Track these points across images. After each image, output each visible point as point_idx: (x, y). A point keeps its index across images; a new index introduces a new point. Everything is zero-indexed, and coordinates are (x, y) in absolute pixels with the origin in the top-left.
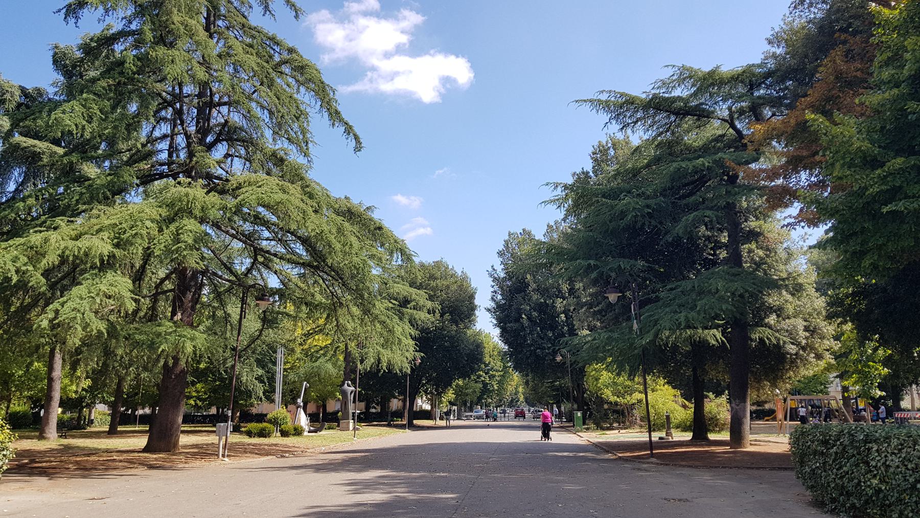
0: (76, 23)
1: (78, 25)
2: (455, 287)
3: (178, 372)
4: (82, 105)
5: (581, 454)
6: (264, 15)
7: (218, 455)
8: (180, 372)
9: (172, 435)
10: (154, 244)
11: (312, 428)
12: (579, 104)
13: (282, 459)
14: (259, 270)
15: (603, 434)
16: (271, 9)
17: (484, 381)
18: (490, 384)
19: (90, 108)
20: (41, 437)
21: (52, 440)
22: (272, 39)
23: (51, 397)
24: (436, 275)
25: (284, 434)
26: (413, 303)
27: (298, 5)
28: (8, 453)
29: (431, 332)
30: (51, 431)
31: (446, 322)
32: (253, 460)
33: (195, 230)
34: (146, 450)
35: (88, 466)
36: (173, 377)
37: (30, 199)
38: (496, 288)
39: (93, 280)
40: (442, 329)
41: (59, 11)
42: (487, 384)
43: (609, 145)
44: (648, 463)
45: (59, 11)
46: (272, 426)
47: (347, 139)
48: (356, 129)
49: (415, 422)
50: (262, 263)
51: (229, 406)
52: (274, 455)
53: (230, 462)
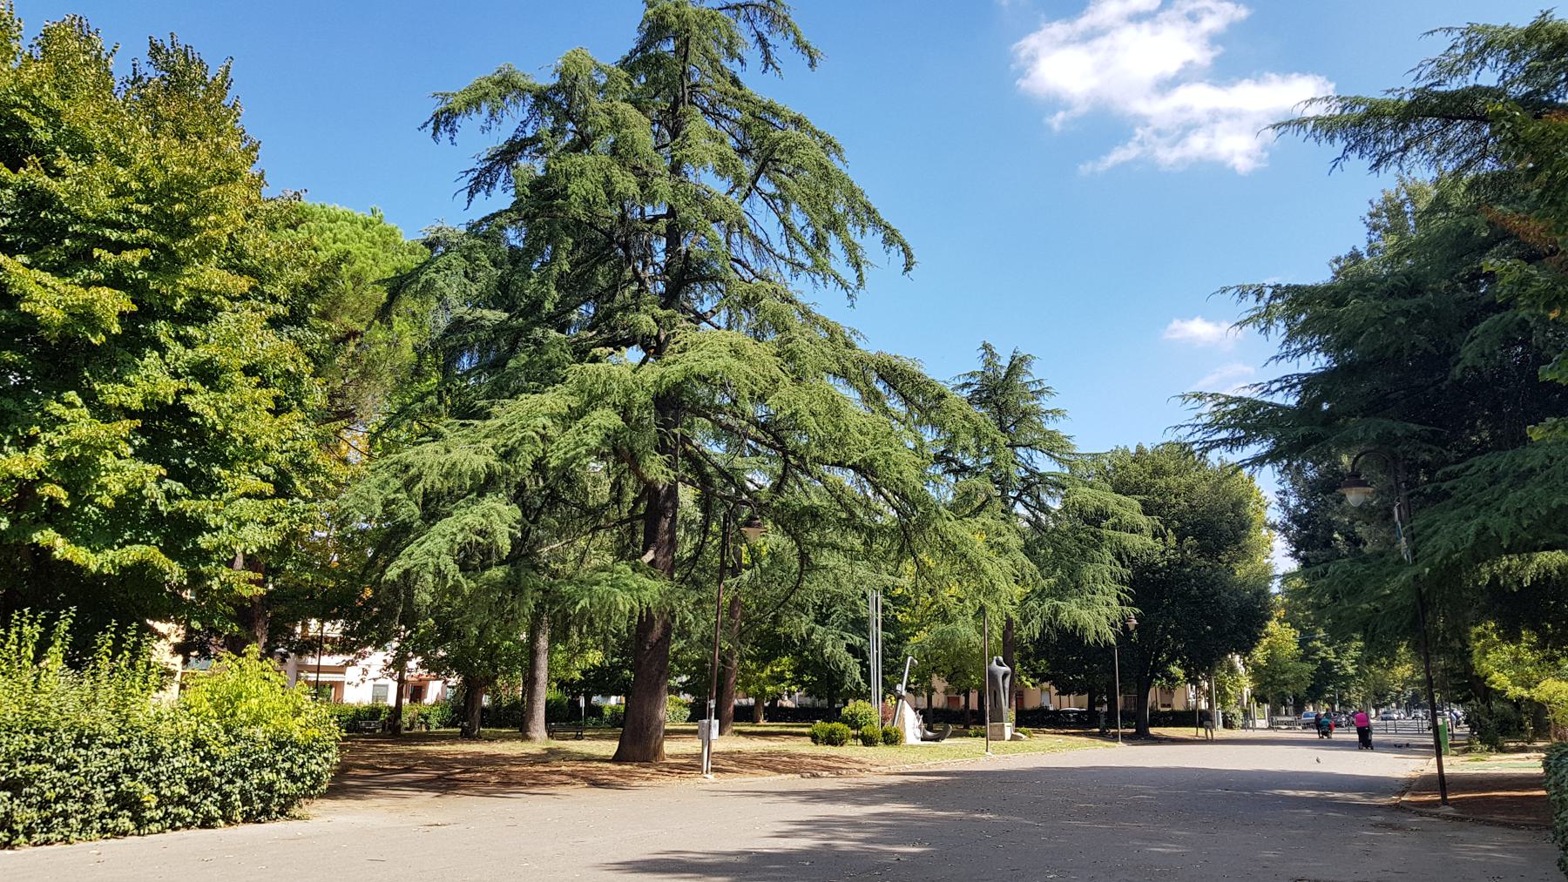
0: (451, 139)
1: (455, 141)
2: (1204, 488)
3: (655, 641)
4: (465, 257)
5: (1336, 795)
6: (764, 72)
7: (700, 768)
8: (658, 641)
9: (651, 737)
10: (552, 451)
11: (929, 733)
12: (1280, 131)
13: (813, 779)
14: (796, 477)
15: (1477, 760)
16: (775, 60)
17: (1325, 658)
18: (1336, 664)
19: (477, 259)
20: (525, 737)
21: (539, 740)
22: (768, 108)
23: (536, 679)
24: (1167, 468)
25: (868, 741)
26: (1112, 520)
27: (813, 46)
28: (330, 755)
29: (1161, 570)
30: (536, 728)
31: (1189, 552)
32: (751, 779)
33: (607, 425)
34: (617, 759)
35: (515, 778)
36: (648, 648)
37: (430, 397)
38: (1287, 485)
39: (468, 508)
40: (1182, 564)
41: (425, 125)
42: (1332, 664)
43: (1403, 196)
44: (1431, 815)
45: (425, 125)
46: (846, 726)
47: (888, 252)
48: (905, 235)
49: (1153, 731)
50: (798, 467)
51: (711, 693)
52: (795, 772)
53: (714, 780)
